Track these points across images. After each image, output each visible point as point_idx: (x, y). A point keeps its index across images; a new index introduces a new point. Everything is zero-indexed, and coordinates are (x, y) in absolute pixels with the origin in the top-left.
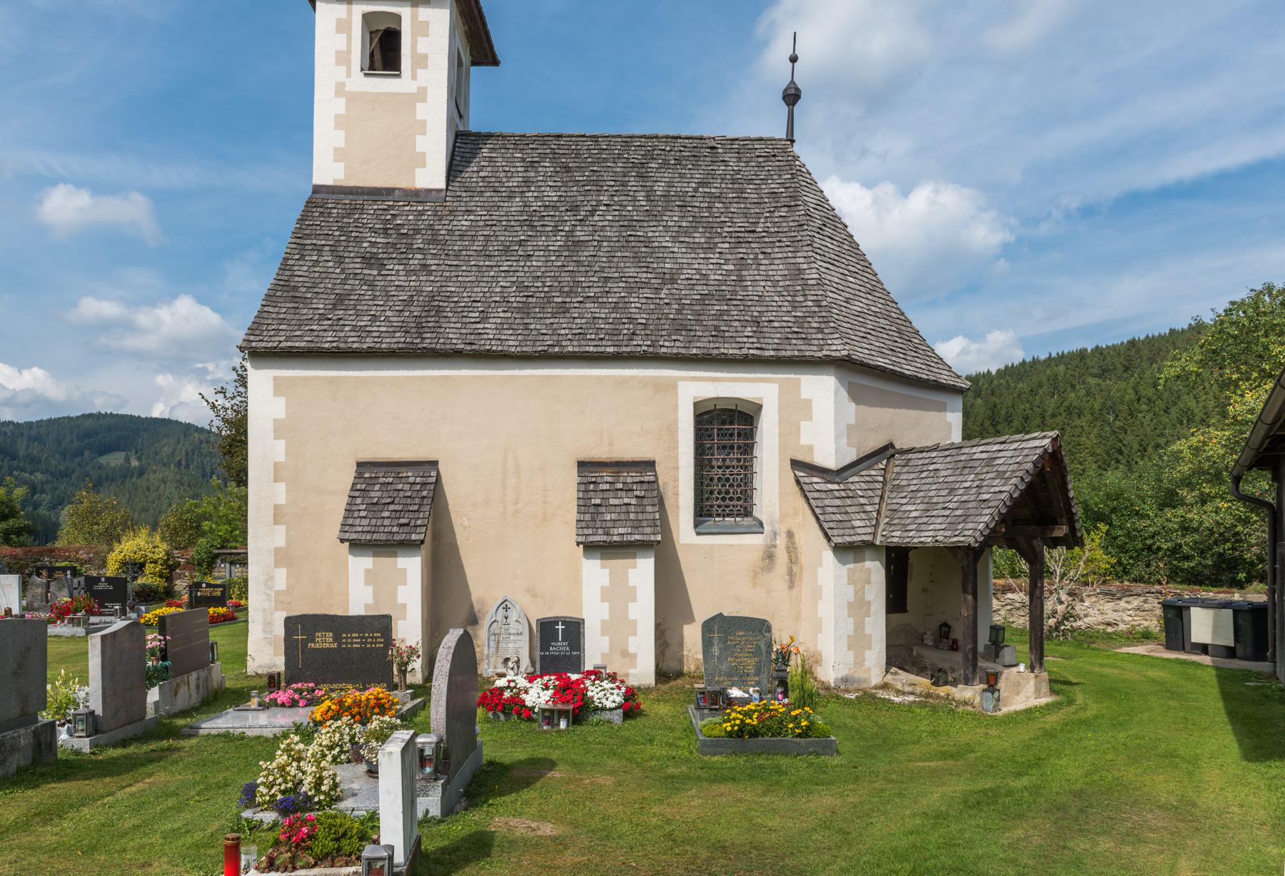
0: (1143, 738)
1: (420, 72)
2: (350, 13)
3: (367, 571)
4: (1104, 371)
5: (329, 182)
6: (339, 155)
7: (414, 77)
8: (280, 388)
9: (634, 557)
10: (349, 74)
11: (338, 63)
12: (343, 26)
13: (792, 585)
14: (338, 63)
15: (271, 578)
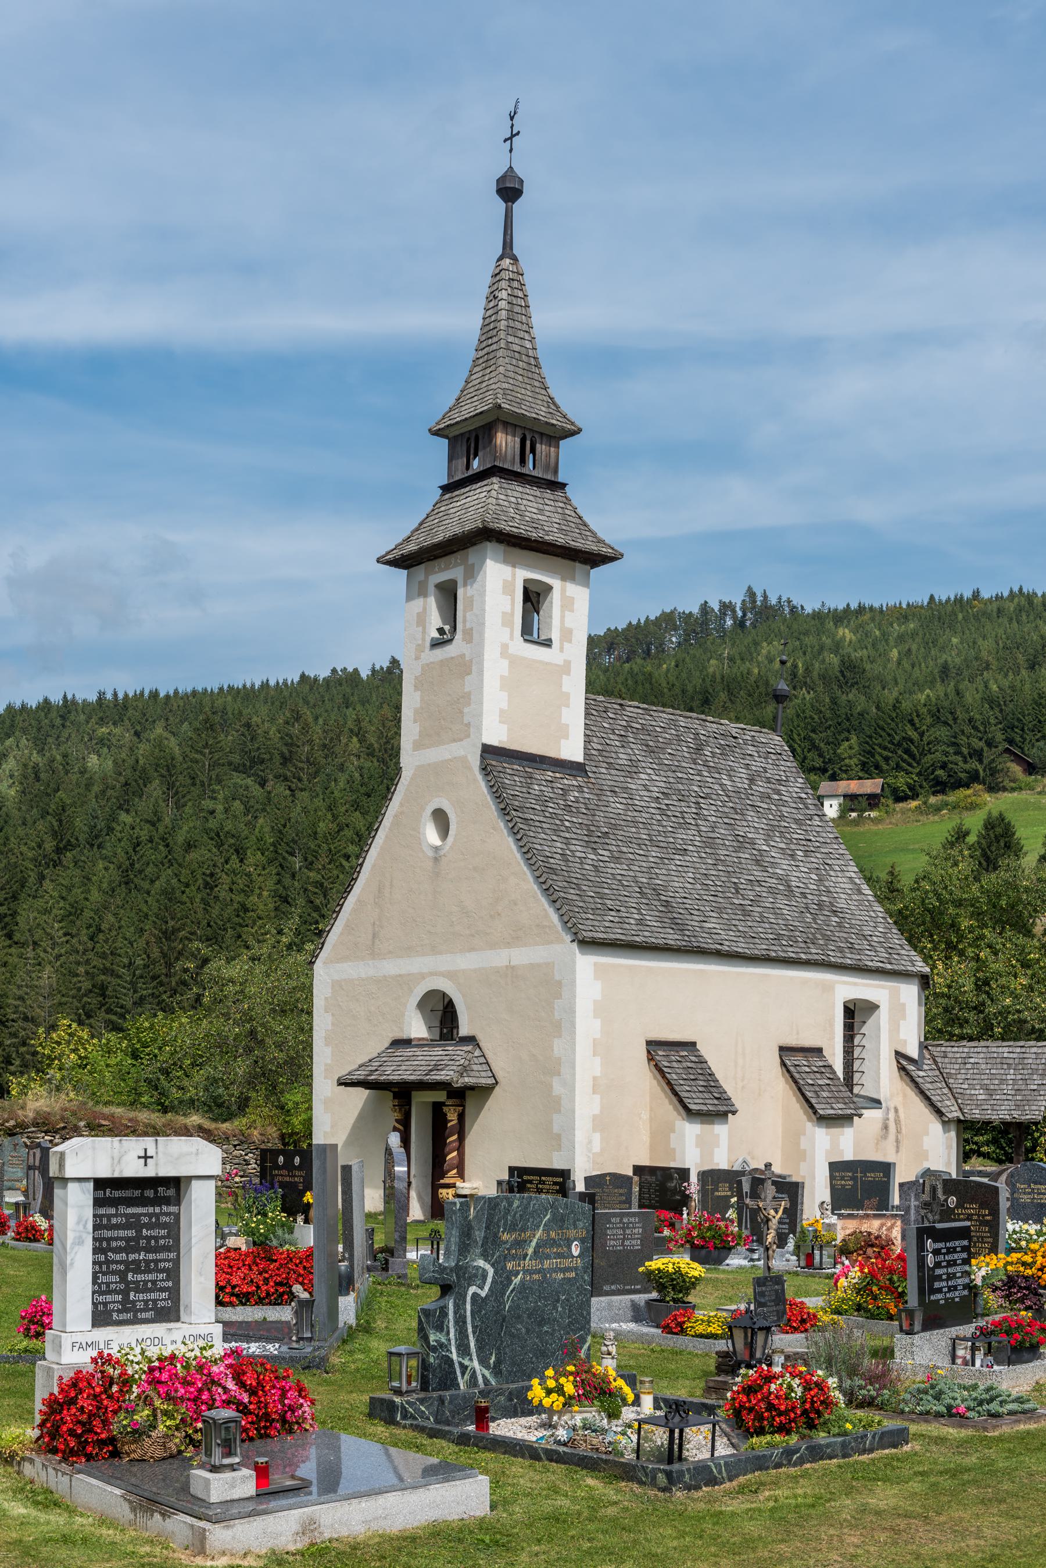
0: (155, 1557)
1: (566, 645)
2: (514, 575)
3: (697, 1136)
4: (253, 761)
5: (495, 743)
6: (504, 717)
7: (562, 649)
8: (599, 972)
9: (713, 1123)
10: (512, 638)
11: (504, 624)
12: (508, 588)
13: (897, 1152)
14: (504, 624)
15: (590, 1142)
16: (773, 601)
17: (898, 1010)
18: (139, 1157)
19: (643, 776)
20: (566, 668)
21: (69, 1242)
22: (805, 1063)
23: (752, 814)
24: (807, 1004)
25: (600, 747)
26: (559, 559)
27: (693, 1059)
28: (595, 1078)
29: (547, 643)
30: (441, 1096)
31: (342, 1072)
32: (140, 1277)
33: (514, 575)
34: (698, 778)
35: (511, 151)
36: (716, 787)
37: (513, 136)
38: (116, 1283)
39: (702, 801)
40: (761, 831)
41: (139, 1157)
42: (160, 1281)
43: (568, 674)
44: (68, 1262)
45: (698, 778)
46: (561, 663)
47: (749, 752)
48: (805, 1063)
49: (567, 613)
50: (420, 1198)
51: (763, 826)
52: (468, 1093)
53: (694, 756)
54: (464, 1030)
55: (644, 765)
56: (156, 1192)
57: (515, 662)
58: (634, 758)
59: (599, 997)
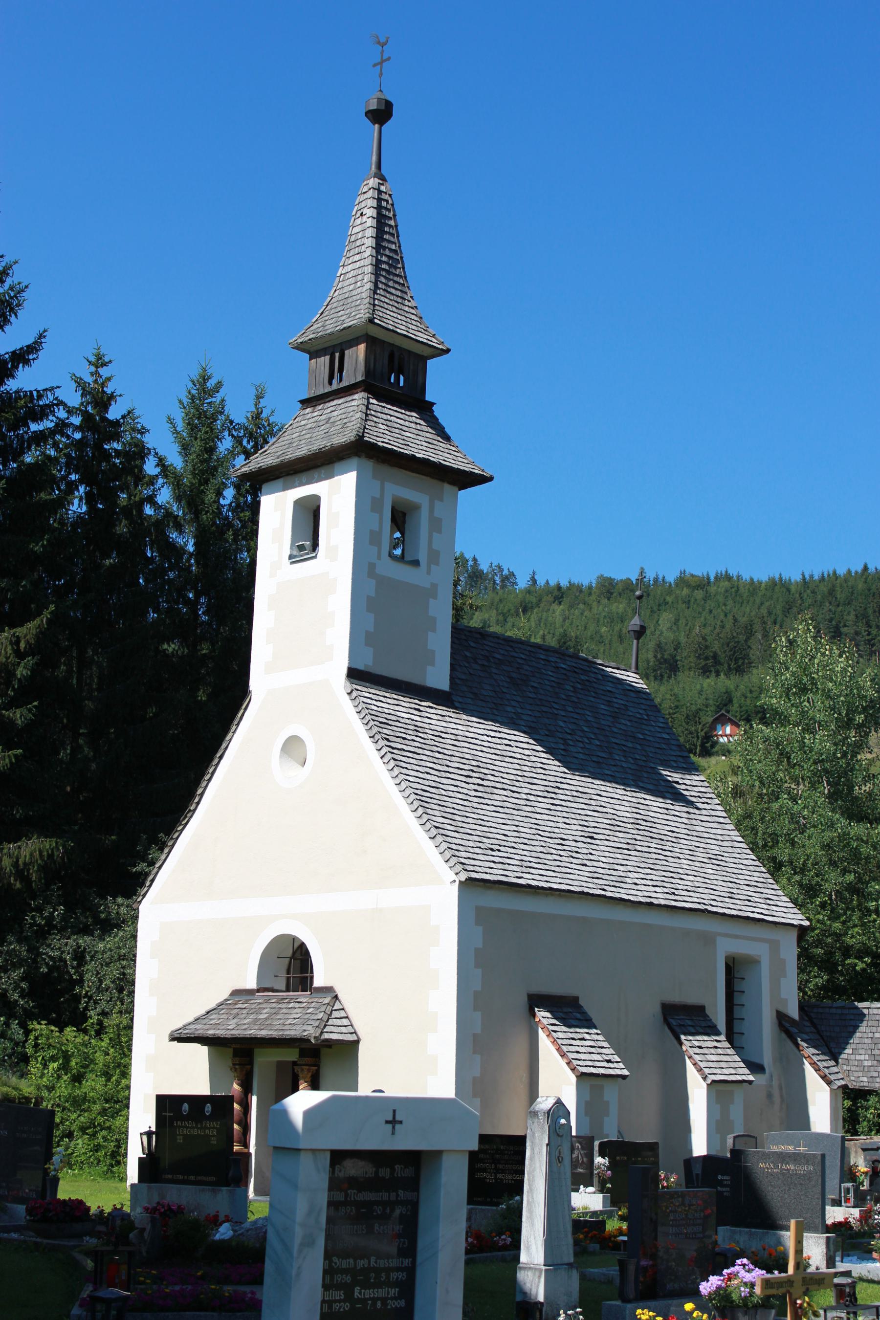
7: (429, 572)
10: (379, 557)
16: (484, 567)
18: (401, 1122)
19: (509, 709)
20: (432, 592)
21: (297, 1241)
22: (690, 1023)
23: (619, 753)
25: (463, 677)
26: (428, 478)
27: (579, 1016)
28: (475, 1035)
29: (416, 563)
30: (291, 1055)
31: (178, 1024)
32: (368, 1293)
34: (563, 713)
35: (381, 75)
36: (581, 723)
37: (381, 63)
38: (340, 1301)
39: (569, 737)
40: (629, 771)
41: (401, 1122)
42: (392, 1299)
43: (435, 597)
44: (294, 1272)
45: (563, 713)
47: (609, 688)
48: (690, 1023)
49: (378, 496)
51: (630, 766)
52: (324, 1051)
53: (557, 690)
54: (318, 982)
55: (508, 696)
56: (393, 1171)
57: (383, 583)
58: (497, 689)
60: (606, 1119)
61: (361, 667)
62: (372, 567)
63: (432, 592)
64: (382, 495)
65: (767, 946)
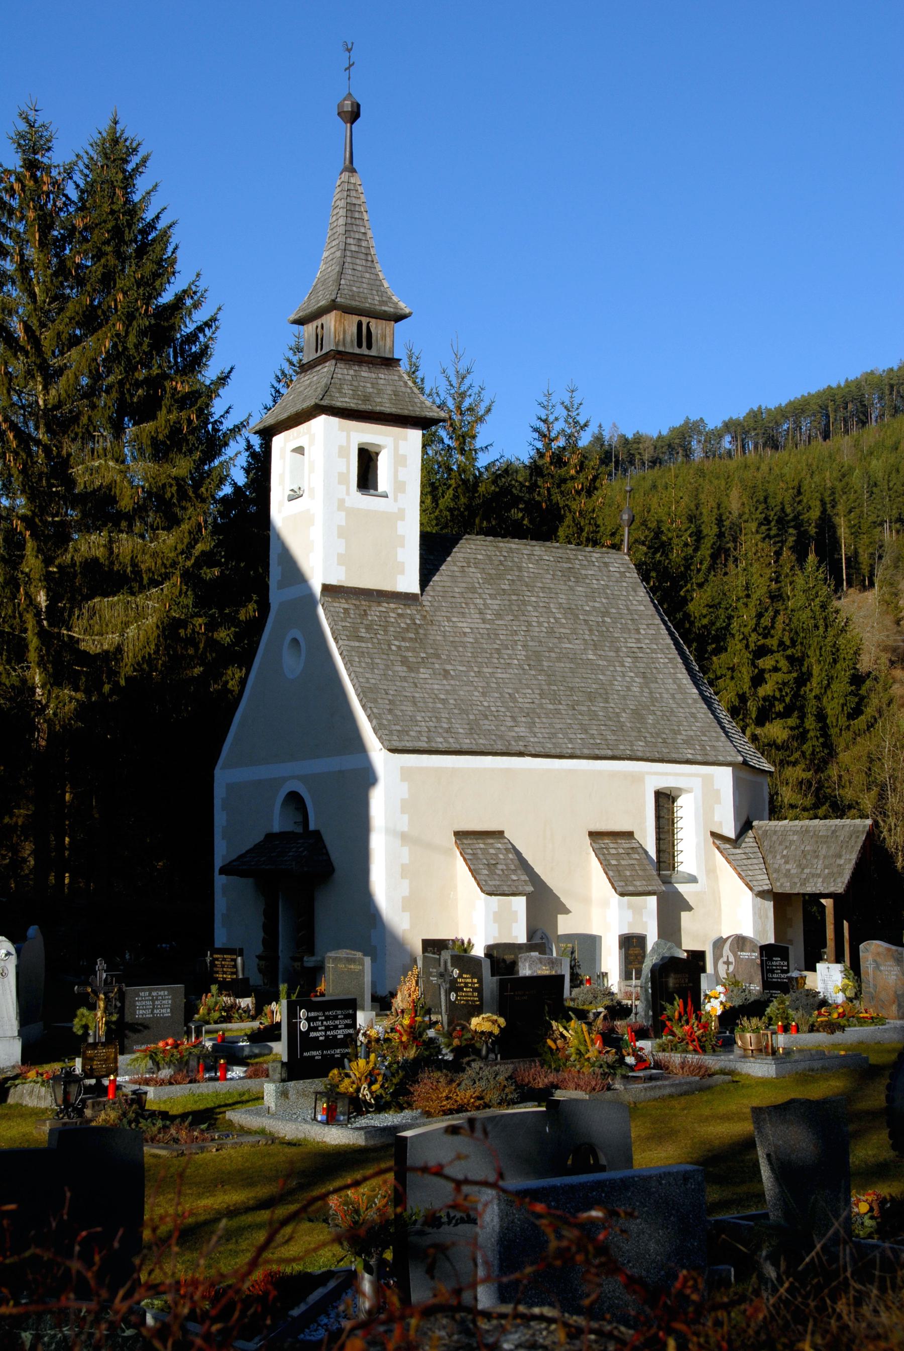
2: (348, 437)
7: (396, 500)
10: (348, 493)
17: (710, 795)
24: (621, 792)
33: (348, 437)
37: (350, 66)
43: (403, 519)
46: (396, 510)
49: (400, 469)
50: (868, 974)
57: (351, 513)
59: (406, 796)
60: (514, 925)
61: (334, 582)
62: (341, 502)
63: (401, 515)
64: (348, 441)
65: (700, 779)
